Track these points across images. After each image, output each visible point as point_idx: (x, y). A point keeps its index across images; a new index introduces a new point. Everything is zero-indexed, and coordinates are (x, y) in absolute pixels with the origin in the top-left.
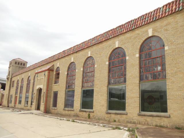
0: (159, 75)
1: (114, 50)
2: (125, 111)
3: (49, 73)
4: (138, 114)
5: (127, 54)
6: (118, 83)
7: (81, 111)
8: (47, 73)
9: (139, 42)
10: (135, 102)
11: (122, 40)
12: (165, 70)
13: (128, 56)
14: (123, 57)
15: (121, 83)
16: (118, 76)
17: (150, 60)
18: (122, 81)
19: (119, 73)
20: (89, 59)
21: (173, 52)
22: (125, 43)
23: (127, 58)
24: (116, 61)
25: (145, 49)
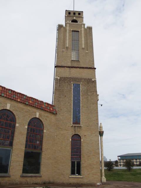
0: (38, 147)
1: (4, 109)
2: (39, 174)
4: (21, 176)
5: (17, 121)
6: (2, 145)
7: (22, 177)
9: (29, 117)
10: (20, 165)
11: (15, 106)
12: (42, 144)
13: (19, 123)
14: (11, 121)
15: (6, 145)
16: (3, 137)
17: (33, 134)
18: (7, 144)
19: (5, 135)
20: (78, 136)
21: (48, 135)
22: (16, 111)
23: (17, 125)
24: (2, 122)
25: (31, 124)
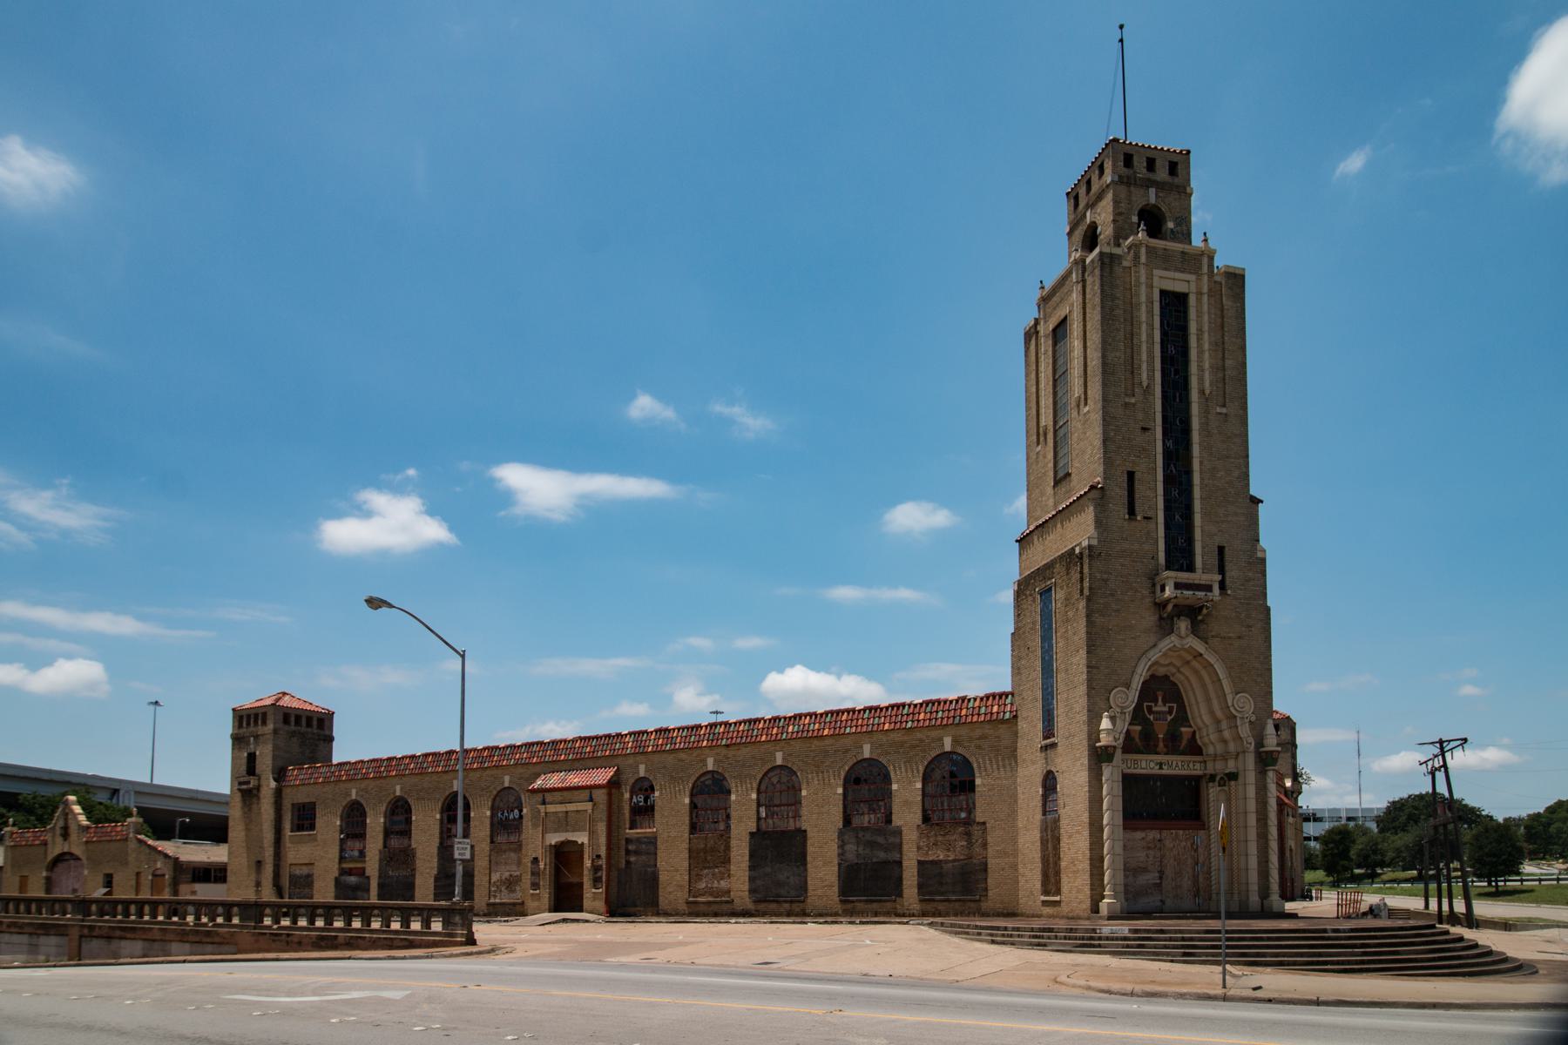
3: (610, 795)
8: (601, 796)
